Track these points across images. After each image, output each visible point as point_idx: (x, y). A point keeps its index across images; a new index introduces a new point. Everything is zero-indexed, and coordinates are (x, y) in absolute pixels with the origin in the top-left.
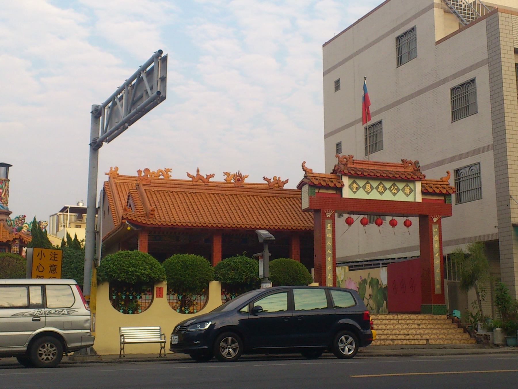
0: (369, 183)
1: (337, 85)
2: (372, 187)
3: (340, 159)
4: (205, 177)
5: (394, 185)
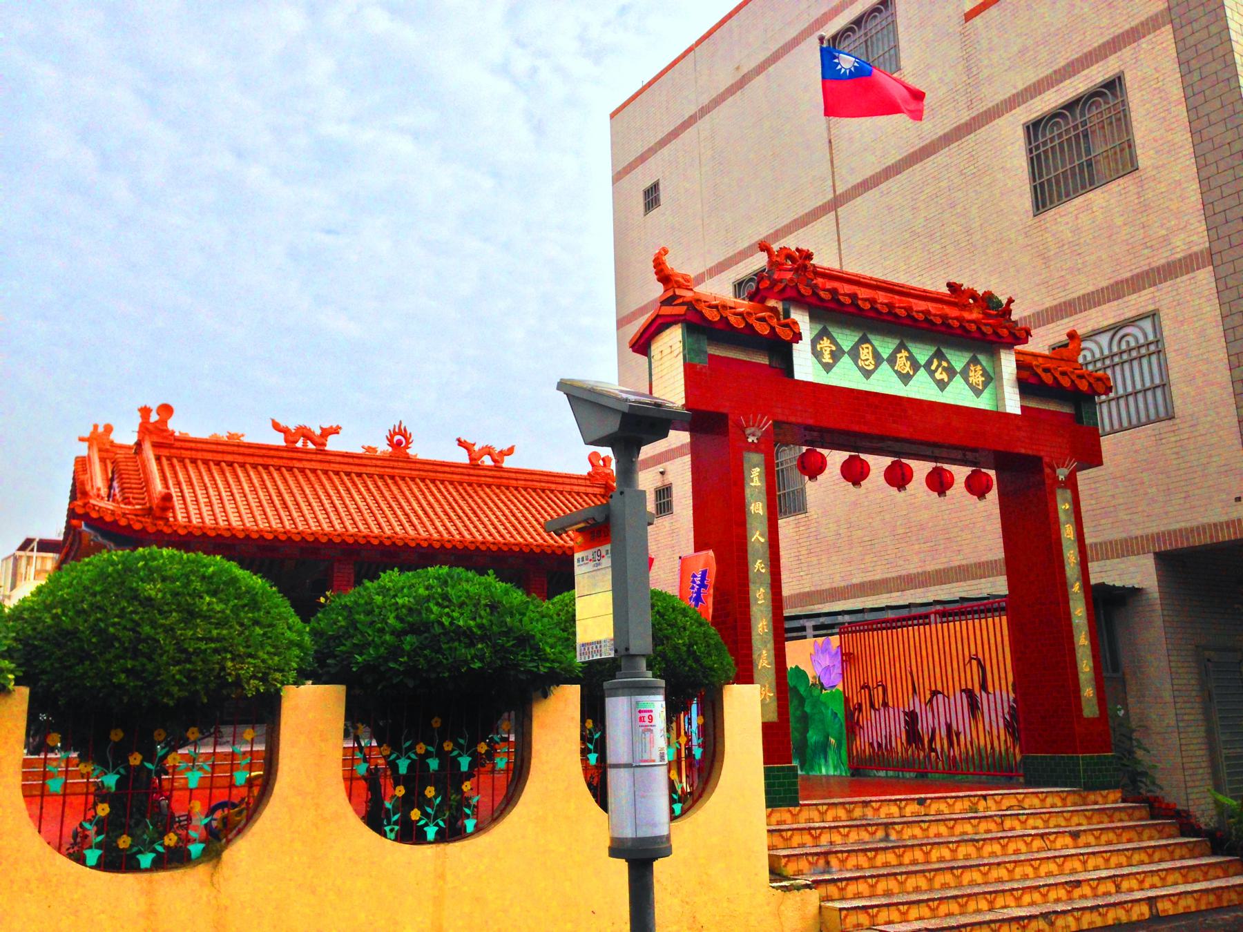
0: (868, 341)
1: (652, 197)
2: (877, 357)
3: (775, 259)
4: (318, 432)
5: (939, 355)
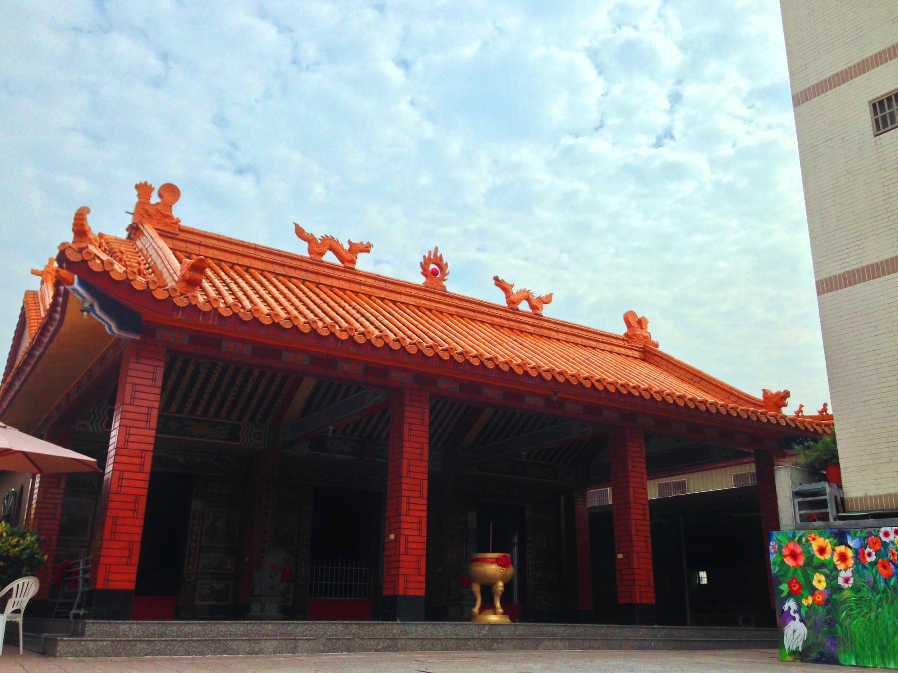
4: (347, 247)
